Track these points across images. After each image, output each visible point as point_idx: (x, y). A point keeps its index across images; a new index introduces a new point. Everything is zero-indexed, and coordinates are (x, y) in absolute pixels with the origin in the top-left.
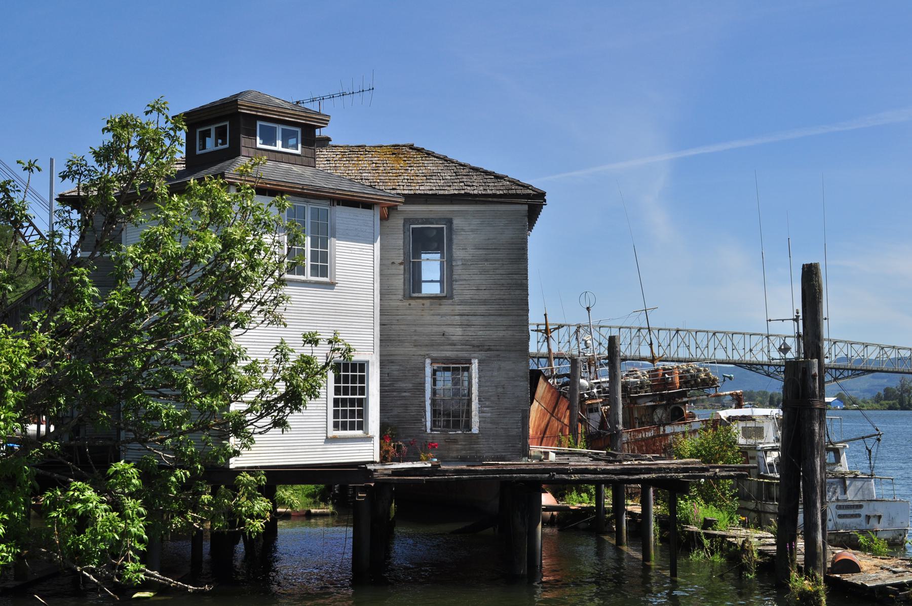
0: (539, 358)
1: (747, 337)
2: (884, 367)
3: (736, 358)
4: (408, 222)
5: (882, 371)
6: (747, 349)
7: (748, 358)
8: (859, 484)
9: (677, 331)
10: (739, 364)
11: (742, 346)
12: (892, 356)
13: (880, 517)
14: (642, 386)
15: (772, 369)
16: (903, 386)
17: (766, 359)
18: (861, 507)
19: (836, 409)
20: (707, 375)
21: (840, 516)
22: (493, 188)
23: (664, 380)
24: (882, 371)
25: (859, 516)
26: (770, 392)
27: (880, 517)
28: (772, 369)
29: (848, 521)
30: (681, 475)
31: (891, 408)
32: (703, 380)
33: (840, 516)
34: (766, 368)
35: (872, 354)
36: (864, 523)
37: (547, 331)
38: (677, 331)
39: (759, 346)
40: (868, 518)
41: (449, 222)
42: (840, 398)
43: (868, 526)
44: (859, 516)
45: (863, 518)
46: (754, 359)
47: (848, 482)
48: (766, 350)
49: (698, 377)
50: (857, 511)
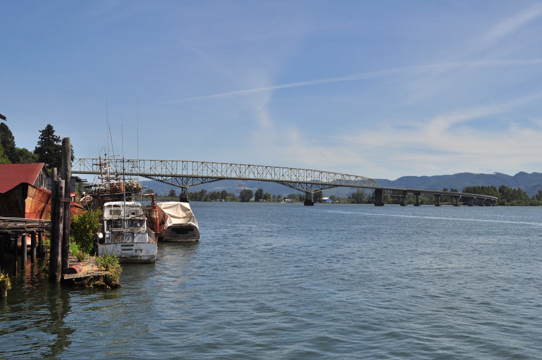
0: (183, 177)
1: (281, 169)
2: (343, 184)
3: (276, 179)
5: (342, 186)
6: (281, 175)
7: (281, 179)
8: (140, 235)
9: (249, 166)
10: (277, 181)
11: (279, 173)
12: (347, 179)
13: (141, 250)
14: (105, 191)
15: (292, 184)
16: (358, 193)
17: (289, 180)
18: (133, 245)
19: (328, 203)
20: (138, 186)
21: (123, 250)
23: (116, 188)
24: (342, 186)
25: (132, 249)
26: (535, 195)
27: (141, 250)
28: (292, 184)
29: (127, 252)
30: (10, 231)
31: (353, 203)
32: (135, 189)
33: (123, 250)
34: (290, 183)
35: (353, 178)
36: (134, 253)
37: (100, 165)
38: (249, 166)
39: (287, 174)
40: (136, 250)
42: (332, 198)
43: (136, 254)
44: (132, 249)
45: (134, 251)
46: (284, 179)
47: (135, 235)
48: (290, 175)
49: (132, 187)
50: (131, 248)
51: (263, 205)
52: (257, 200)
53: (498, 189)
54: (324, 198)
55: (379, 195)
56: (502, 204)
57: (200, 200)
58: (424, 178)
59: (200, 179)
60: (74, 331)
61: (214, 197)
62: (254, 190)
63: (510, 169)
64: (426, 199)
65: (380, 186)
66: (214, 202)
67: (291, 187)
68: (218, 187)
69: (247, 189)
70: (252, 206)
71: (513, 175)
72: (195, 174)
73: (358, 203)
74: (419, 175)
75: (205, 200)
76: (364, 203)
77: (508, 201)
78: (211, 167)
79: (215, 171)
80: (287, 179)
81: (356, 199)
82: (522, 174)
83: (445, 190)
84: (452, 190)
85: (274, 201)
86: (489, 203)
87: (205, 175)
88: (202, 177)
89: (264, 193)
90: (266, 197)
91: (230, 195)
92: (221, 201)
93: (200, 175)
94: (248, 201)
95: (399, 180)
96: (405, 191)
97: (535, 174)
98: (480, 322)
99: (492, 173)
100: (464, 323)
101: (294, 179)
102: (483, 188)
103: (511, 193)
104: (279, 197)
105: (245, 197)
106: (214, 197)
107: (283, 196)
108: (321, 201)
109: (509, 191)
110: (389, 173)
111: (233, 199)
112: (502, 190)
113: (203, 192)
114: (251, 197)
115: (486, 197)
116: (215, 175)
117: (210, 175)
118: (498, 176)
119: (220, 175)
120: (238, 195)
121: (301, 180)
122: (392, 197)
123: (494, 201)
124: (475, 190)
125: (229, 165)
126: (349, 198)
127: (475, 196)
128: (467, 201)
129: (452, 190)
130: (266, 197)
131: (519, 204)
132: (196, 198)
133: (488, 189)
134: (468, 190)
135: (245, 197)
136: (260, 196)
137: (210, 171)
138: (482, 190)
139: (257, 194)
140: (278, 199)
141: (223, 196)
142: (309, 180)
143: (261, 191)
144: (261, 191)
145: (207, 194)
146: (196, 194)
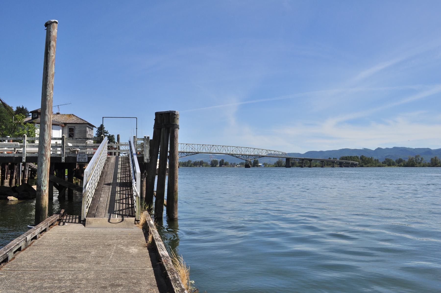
3: (229, 153)
4: (68, 127)
7: (231, 153)
22: (82, 122)
35: (273, 152)
41: (75, 127)
51: (224, 168)
52: (221, 166)
53: (359, 157)
54: (260, 164)
55: (289, 162)
56: (362, 166)
57: (187, 166)
58: (321, 152)
59: (186, 154)
60: (146, 222)
61: (196, 164)
62: (219, 160)
63: (373, 147)
64: (318, 163)
65: (288, 157)
66: (196, 167)
67: (237, 157)
68: (197, 159)
69: (214, 159)
70: (218, 168)
71: (374, 149)
72: (182, 151)
73: (279, 166)
74: (318, 150)
75: (191, 166)
76: (283, 166)
77: (365, 164)
78: (191, 147)
79: (193, 149)
80: (235, 153)
81: (278, 165)
82: (379, 149)
83: (330, 158)
84: (334, 158)
85: (230, 166)
86: (353, 165)
87: (188, 151)
88: (186, 153)
89: (225, 162)
90: (226, 164)
91: (205, 163)
92: (200, 166)
93: (185, 151)
94: (215, 166)
95: (306, 153)
96: (303, 159)
97: (387, 149)
98: (353, 213)
99: (361, 149)
100: (309, 207)
101: (239, 153)
102: (351, 157)
103: (367, 160)
104: (234, 164)
105: (214, 164)
106: (196, 164)
107: (237, 163)
108: (257, 166)
109: (366, 158)
110: (300, 149)
111: (207, 165)
112: (362, 158)
113: (189, 162)
114: (217, 164)
115: (351, 162)
116: (194, 151)
117: (191, 151)
118: (365, 150)
119: (196, 151)
120: (209, 163)
121: (243, 153)
122: (299, 163)
123: (356, 164)
124: (346, 158)
125: (185, 145)
126: (275, 164)
127: (344, 161)
128: (341, 165)
129: (334, 158)
130: (226, 164)
131: (371, 166)
132: (185, 165)
133: (354, 157)
134: (342, 158)
135: (214, 164)
136: (222, 164)
137: (191, 149)
138: (351, 158)
139: (220, 162)
140: (233, 165)
141: (201, 164)
142: (247, 153)
143: (223, 160)
144: (223, 160)
145: (192, 162)
146: (185, 163)
